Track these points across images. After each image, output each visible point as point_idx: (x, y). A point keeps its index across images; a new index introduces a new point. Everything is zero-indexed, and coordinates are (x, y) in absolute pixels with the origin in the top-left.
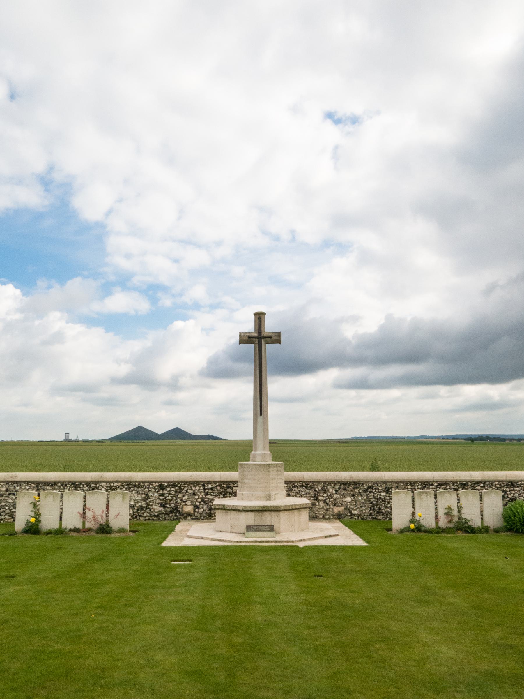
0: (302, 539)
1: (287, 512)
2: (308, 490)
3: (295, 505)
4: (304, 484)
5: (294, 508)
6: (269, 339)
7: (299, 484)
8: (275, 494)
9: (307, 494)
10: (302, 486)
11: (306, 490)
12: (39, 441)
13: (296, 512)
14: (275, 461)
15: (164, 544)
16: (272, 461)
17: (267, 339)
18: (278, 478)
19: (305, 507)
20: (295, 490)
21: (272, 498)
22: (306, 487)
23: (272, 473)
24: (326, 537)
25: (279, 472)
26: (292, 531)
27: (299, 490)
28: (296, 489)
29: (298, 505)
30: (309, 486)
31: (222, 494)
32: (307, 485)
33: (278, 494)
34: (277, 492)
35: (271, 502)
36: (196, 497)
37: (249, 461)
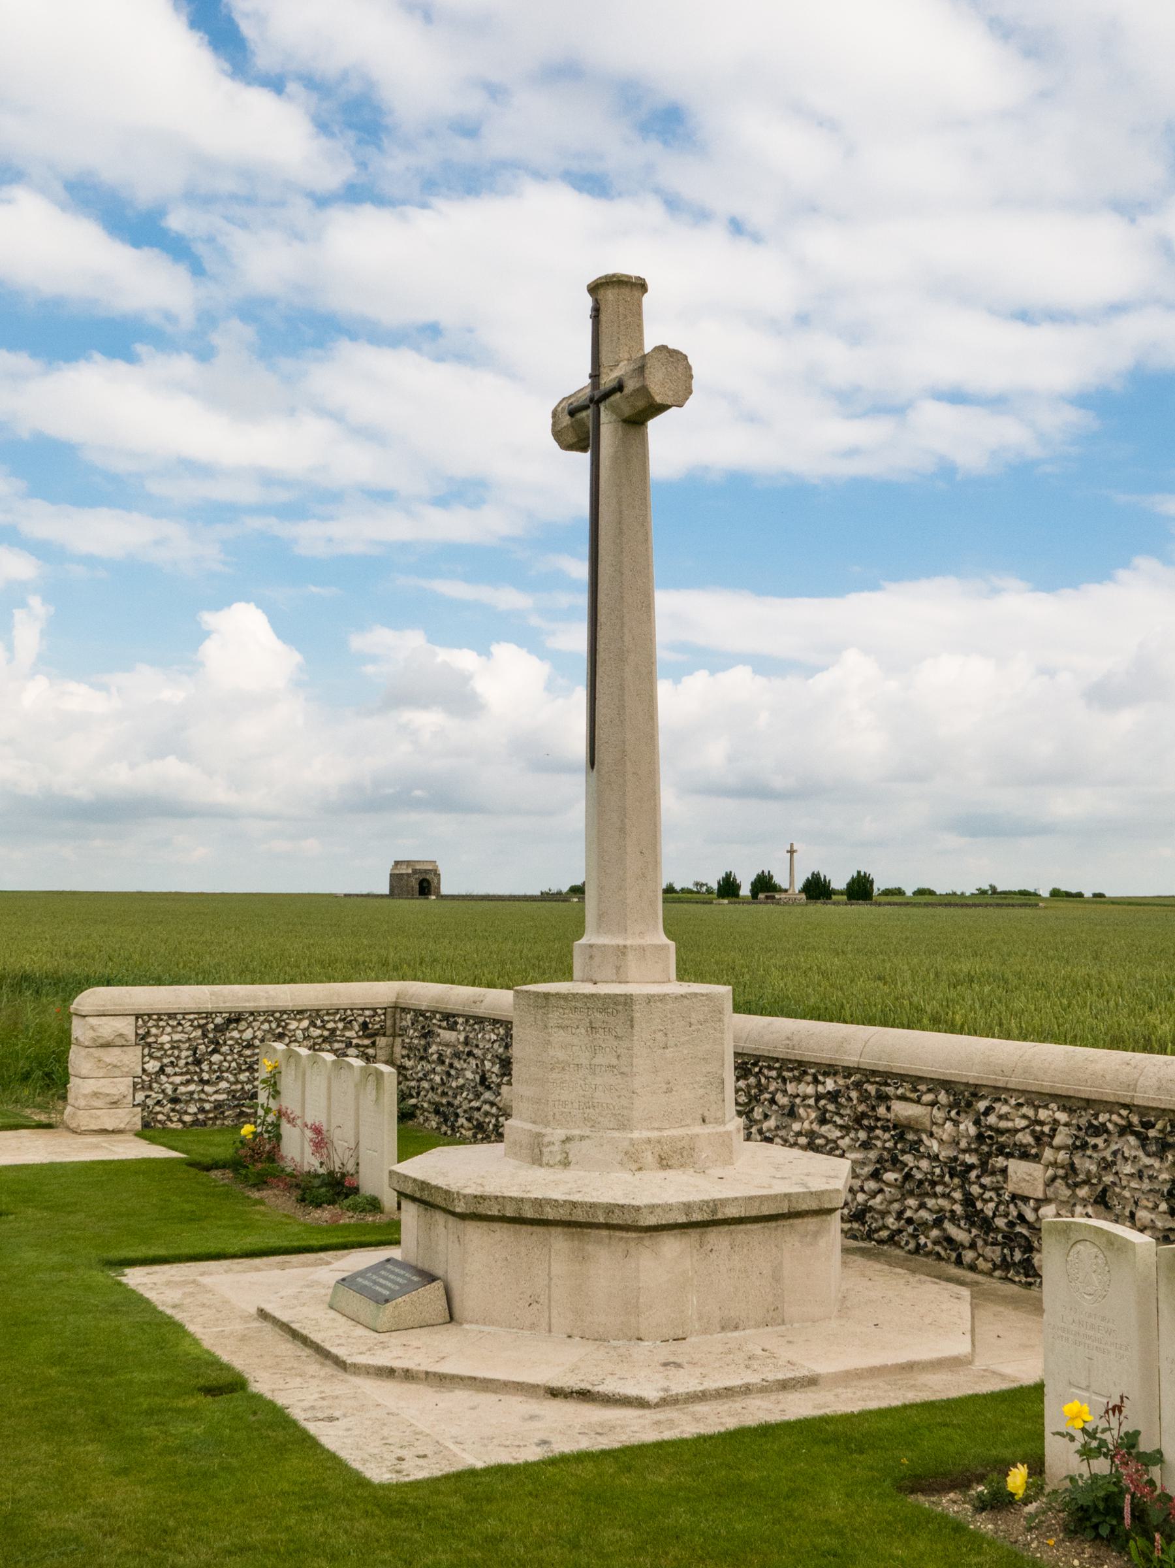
0: (396, 1364)
1: (502, 1232)
2: (1148, 1155)
3: (538, 1203)
4: (1135, 1119)
5: (529, 1213)
6: (618, 395)
7: (1115, 1117)
8: (568, 1140)
9: (1140, 1175)
10: (1125, 1130)
11: (1141, 1154)
12: (346, 895)
13: (559, 1241)
14: (701, 978)
15: (135, 1278)
16: (680, 978)
17: (612, 399)
18: (596, 1061)
19: (602, 1220)
20: (1095, 1147)
21: (554, 1152)
22: (1143, 1140)
23: (559, 1036)
24: (554, 1393)
25: (600, 1035)
26: (533, 1326)
27: (1114, 1147)
28: (1099, 1141)
29: (555, 1204)
30: (1152, 1133)
31: (862, 1127)
32: (1149, 1125)
33: (582, 1138)
34: (586, 1132)
35: (569, 1175)
36: (796, 1127)
37: (566, 974)
